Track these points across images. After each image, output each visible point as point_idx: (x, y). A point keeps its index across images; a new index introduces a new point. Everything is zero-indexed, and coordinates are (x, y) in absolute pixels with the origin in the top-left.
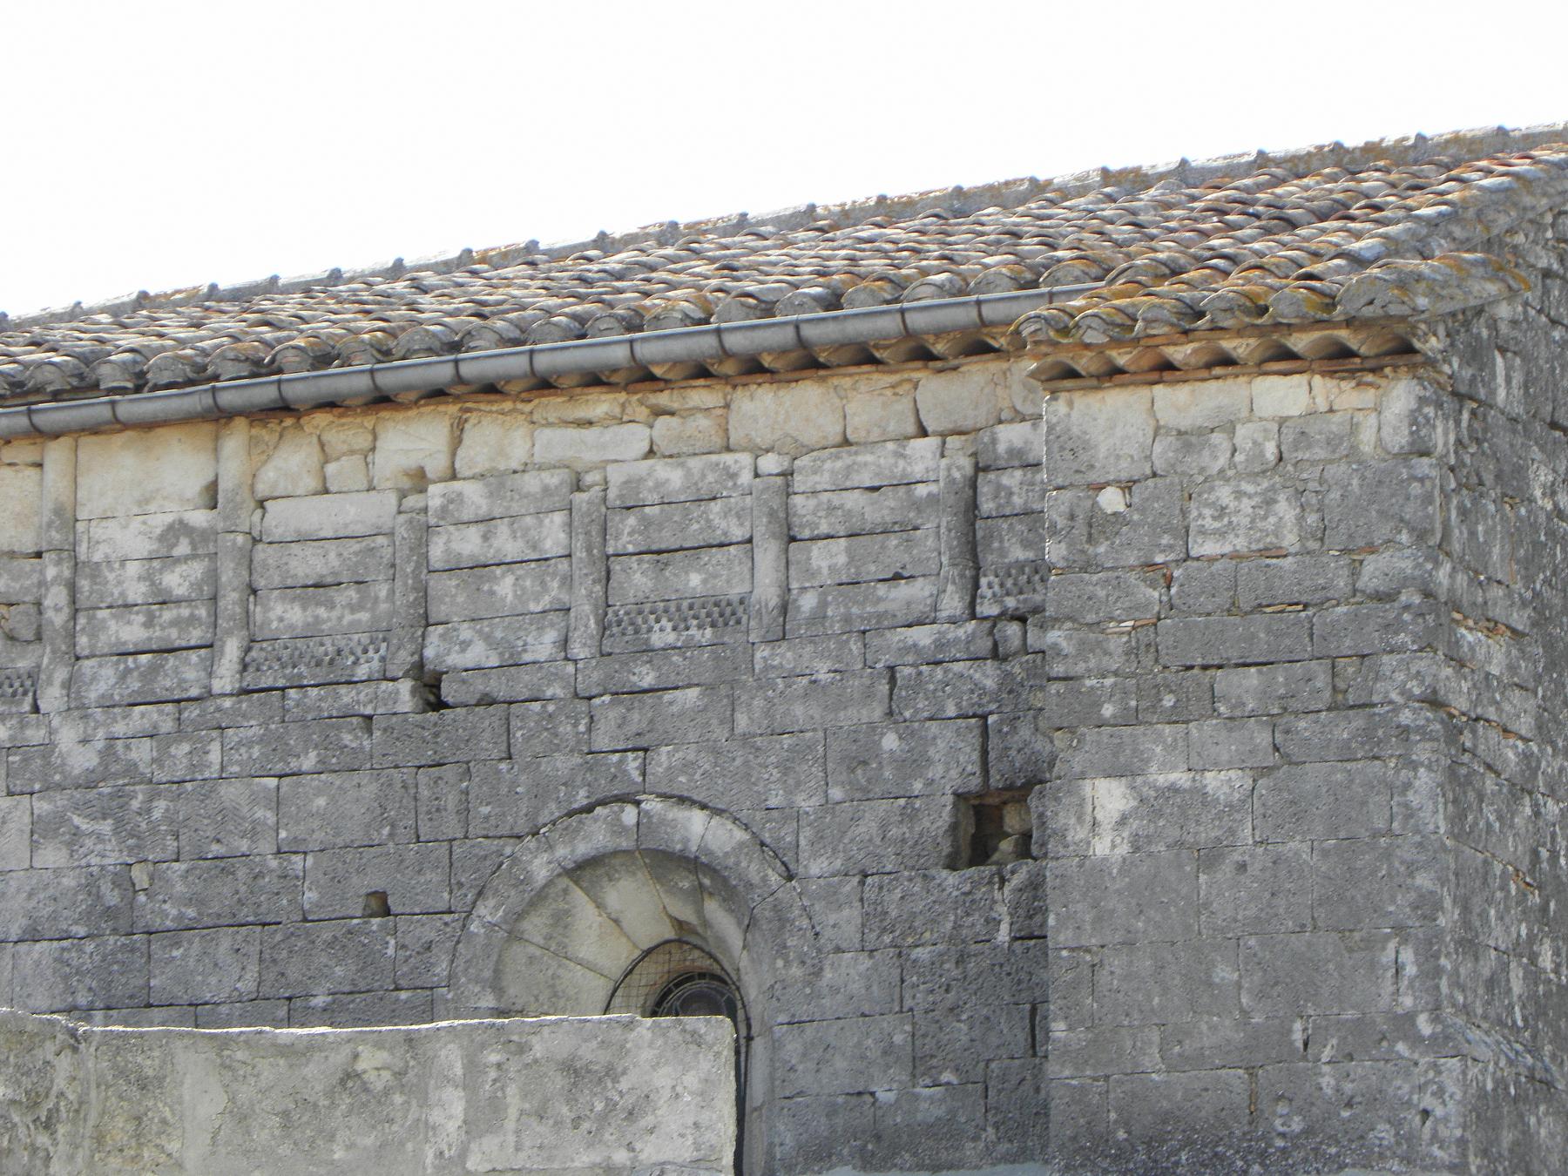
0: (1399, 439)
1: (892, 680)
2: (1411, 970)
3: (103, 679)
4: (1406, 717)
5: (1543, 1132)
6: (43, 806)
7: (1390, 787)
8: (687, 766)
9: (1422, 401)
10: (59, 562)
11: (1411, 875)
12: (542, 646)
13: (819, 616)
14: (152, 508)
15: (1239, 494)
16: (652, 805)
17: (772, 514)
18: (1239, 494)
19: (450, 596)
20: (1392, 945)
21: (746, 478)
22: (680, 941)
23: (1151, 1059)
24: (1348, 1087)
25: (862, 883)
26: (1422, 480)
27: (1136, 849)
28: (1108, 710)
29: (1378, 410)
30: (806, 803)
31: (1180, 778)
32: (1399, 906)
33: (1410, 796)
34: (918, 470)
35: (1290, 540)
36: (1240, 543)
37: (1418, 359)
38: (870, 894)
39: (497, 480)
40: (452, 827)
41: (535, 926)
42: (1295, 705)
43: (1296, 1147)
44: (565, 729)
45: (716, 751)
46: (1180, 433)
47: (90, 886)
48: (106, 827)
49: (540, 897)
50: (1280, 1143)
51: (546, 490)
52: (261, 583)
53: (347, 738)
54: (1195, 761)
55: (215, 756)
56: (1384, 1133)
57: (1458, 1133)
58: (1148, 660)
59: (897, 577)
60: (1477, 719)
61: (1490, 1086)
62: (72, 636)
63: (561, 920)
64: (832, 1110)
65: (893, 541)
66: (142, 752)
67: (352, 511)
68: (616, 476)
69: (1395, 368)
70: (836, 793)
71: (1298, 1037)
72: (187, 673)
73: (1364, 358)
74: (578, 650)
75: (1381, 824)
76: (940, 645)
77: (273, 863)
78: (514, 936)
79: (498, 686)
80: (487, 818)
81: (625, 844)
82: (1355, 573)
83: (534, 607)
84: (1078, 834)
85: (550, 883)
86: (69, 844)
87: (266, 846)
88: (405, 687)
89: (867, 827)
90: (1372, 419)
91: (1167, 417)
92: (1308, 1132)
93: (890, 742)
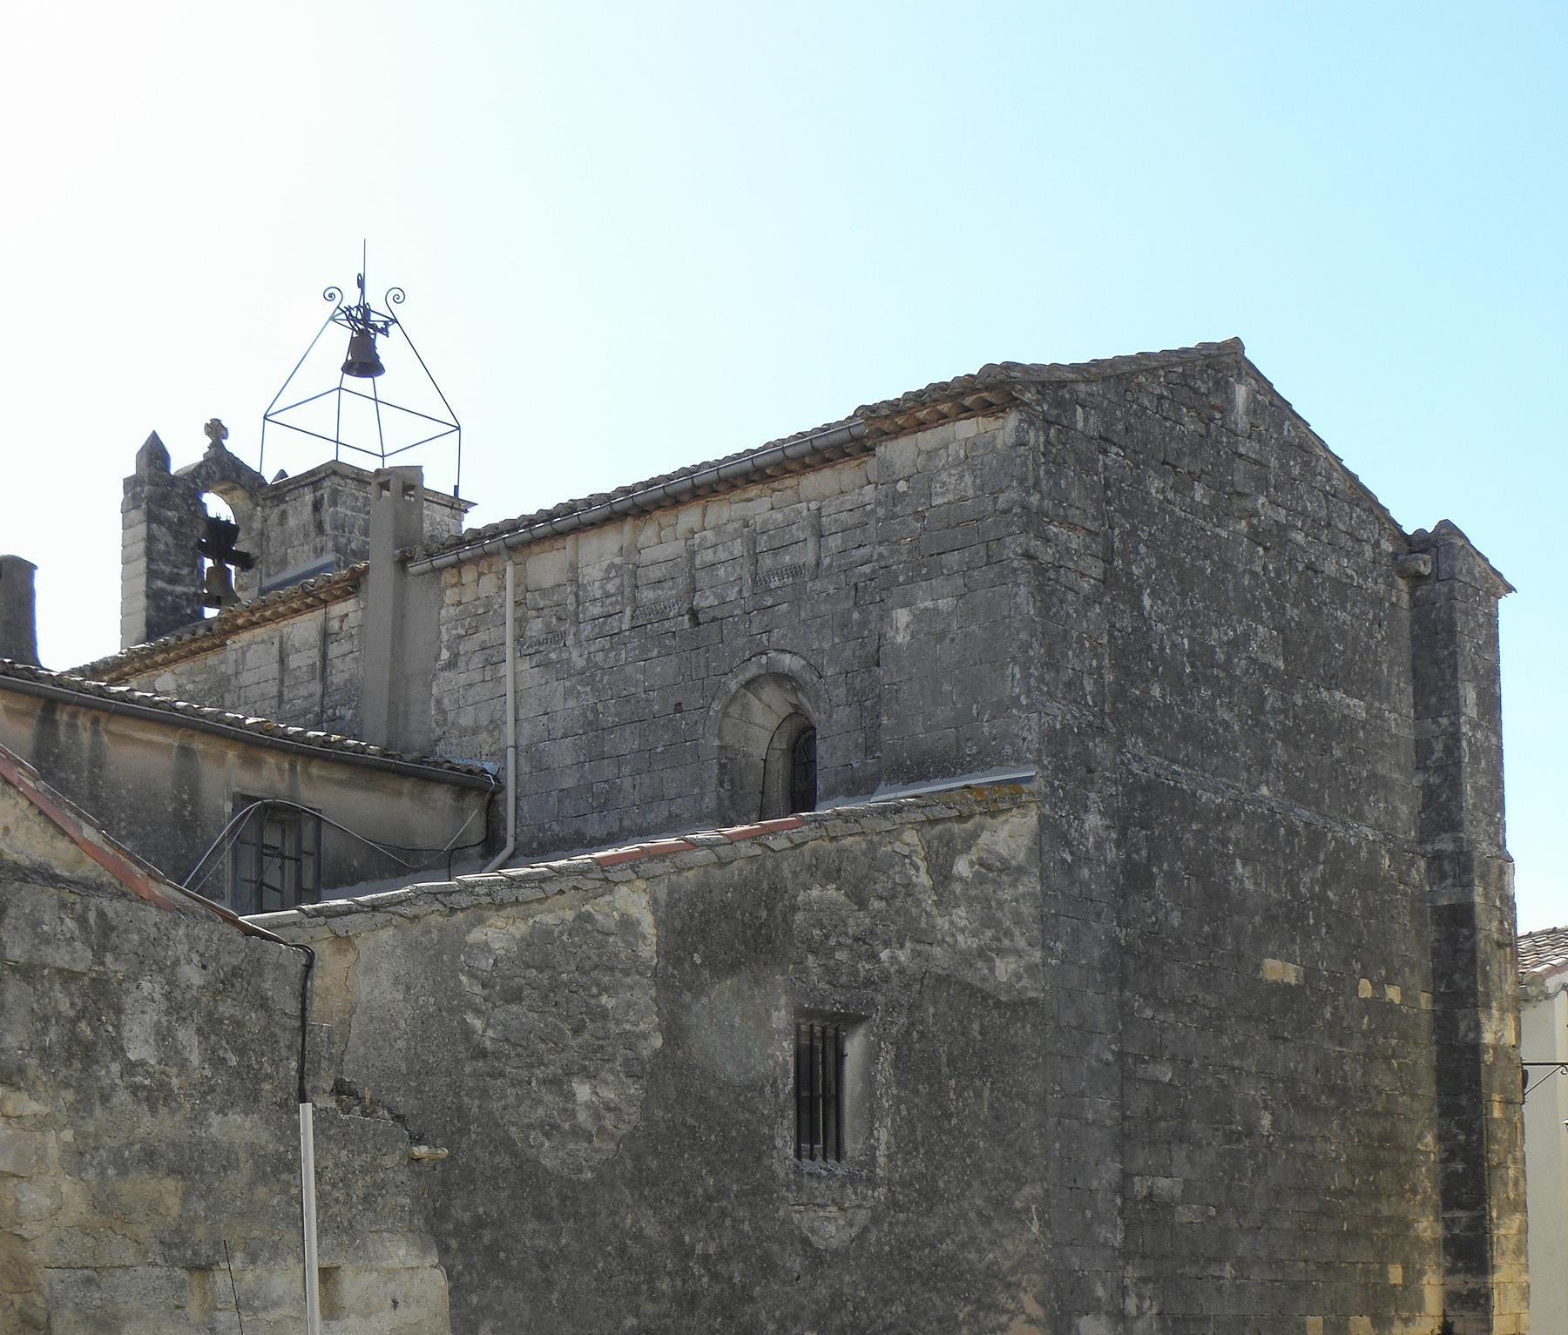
0: (1011, 440)
1: (856, 590)
2: (1018, 676)
3: (587, 630)
4: (1016, 564)
5: (1098, 750)
6: (568, 684)
7: (1009, 596)
8: (784, 636)
9: (1021, 421)
10: (571, 585)
11: (1018, 634)
12: (732, 594)
13: (830, 566)
14: (603, 559)
15: (950, 475)
16: (772, 654)
17: (813, 526)
18: (950, 475)
19: (703, 579)
20: (1011, 666)
21: (805, 513)
22: (796, 713)
23: (920, 728)
24: (994, 731)
25: (846, 676)
26: (1020, 457)
27: (913, 637)
28: (901, 579)
29: (1003, 428)
30: (826, 646)
31: (929, 604)
32: (1013, 649)
33: (1018, 599)
34: (867, 499)
35: (970, 493)
36: (950, 497)
37: (1018, 402)
38: (849, 681)
39: (717, 529)
40: (703, 673)
41: (735, 711)
42: (972, 565)
43: (975, 760)
44: (741, 627)
45: (794, 629)
46: (928, 452)
47: (584, 714)
48: (588, 689)
49: (734, 698)
50: (968, 759)
51: (735, 529)
52: (639, 584)
53: (667, 642)
54: (935, 596)
55: (623, 656)
56: (1008, 750)
57: (1037, 746)
58: (916, 554)
59: (860, 546)
60: (1060, 567)
61: (1058, 726)
62: (577, 614)
63: (746, 707)
64: (837, 774)
65: (858, 531)
66: (600, 657)
67: (669, 549)
68: (759, 519)
69: (1010, 408)
70: (837, 640)
71: (975, 712)
72: (614, 623)
73: (998, 405)
74: (746, 594)
75: (1006, 614)
76: (874, 572)
77: (643, 696)
78: (725, 715)
79: (718, 613)
80: (715, 668)
81: (762, 672)
82: (995, 503)
83: (732, 579)
84: (890, 634)
85: (737, 691)
86: (577, 698)
87: (641, 690)
88: (687, 617)
89: (848, 653)
90: (1001, 433)
91: (924, 447)
92: (979, 753)
93: (856, 615)
